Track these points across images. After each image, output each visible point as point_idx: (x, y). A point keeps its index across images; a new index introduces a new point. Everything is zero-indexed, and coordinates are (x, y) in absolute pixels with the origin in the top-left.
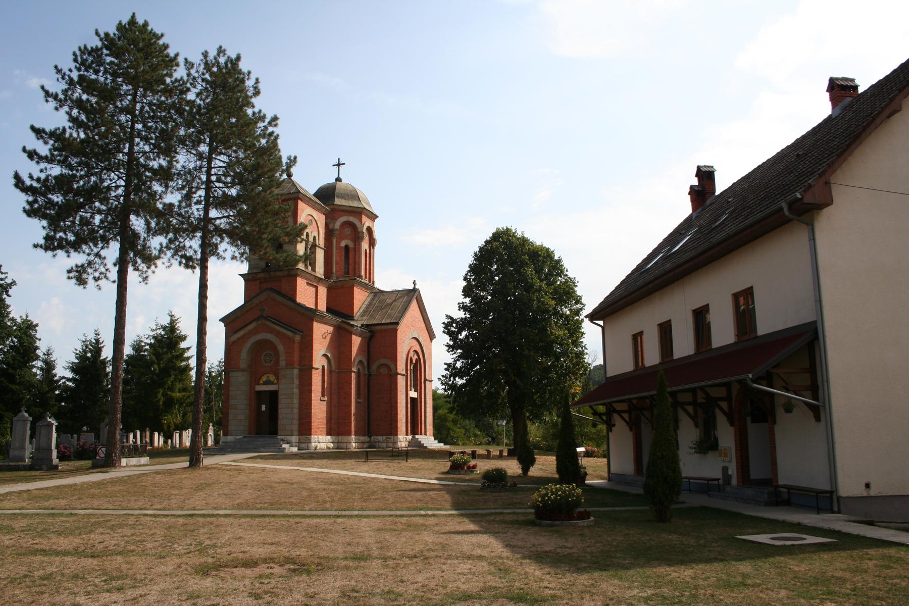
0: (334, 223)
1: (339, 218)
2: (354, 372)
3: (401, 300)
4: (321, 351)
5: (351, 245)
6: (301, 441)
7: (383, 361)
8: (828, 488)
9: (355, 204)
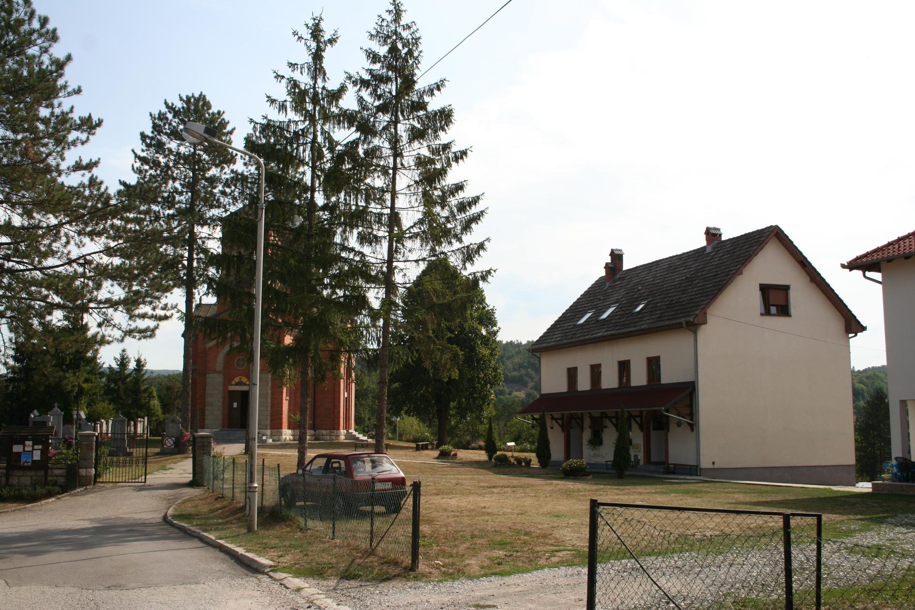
8: (695, 464)
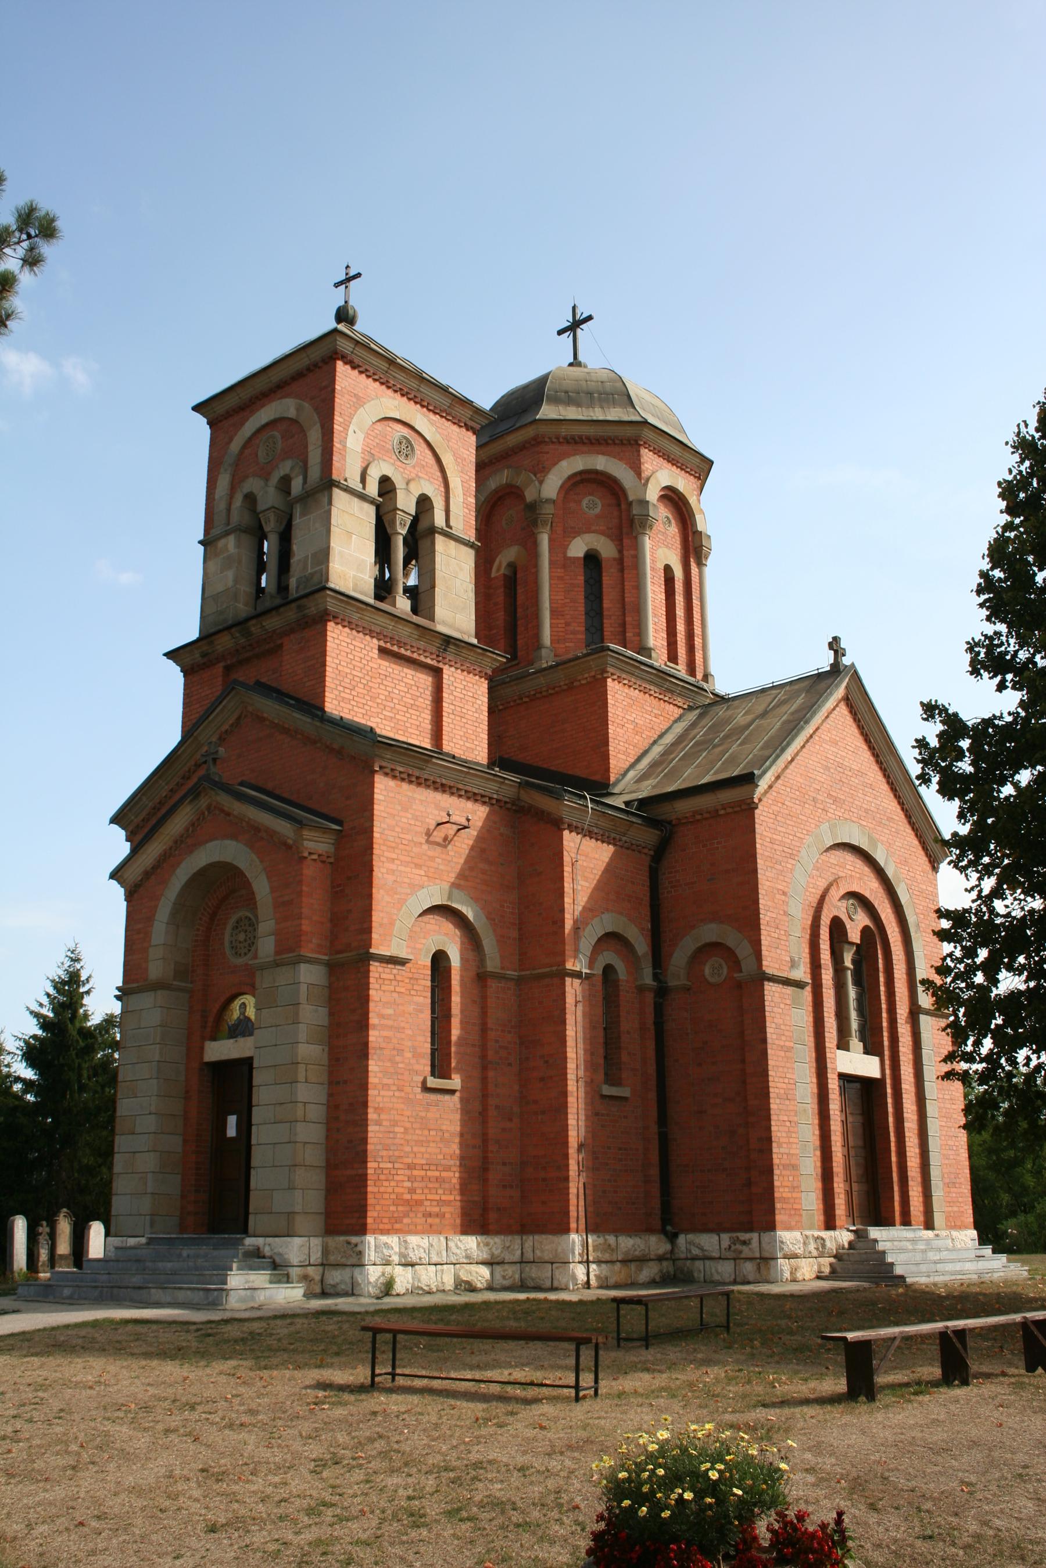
0: (541, 482)
1: (555, 464)
2: (577, 975)
3: (784, 709)
4: (422, 894)
5: (606, 549)
6: (332, 1259)
7: (710, 932)
9: (614, 414)
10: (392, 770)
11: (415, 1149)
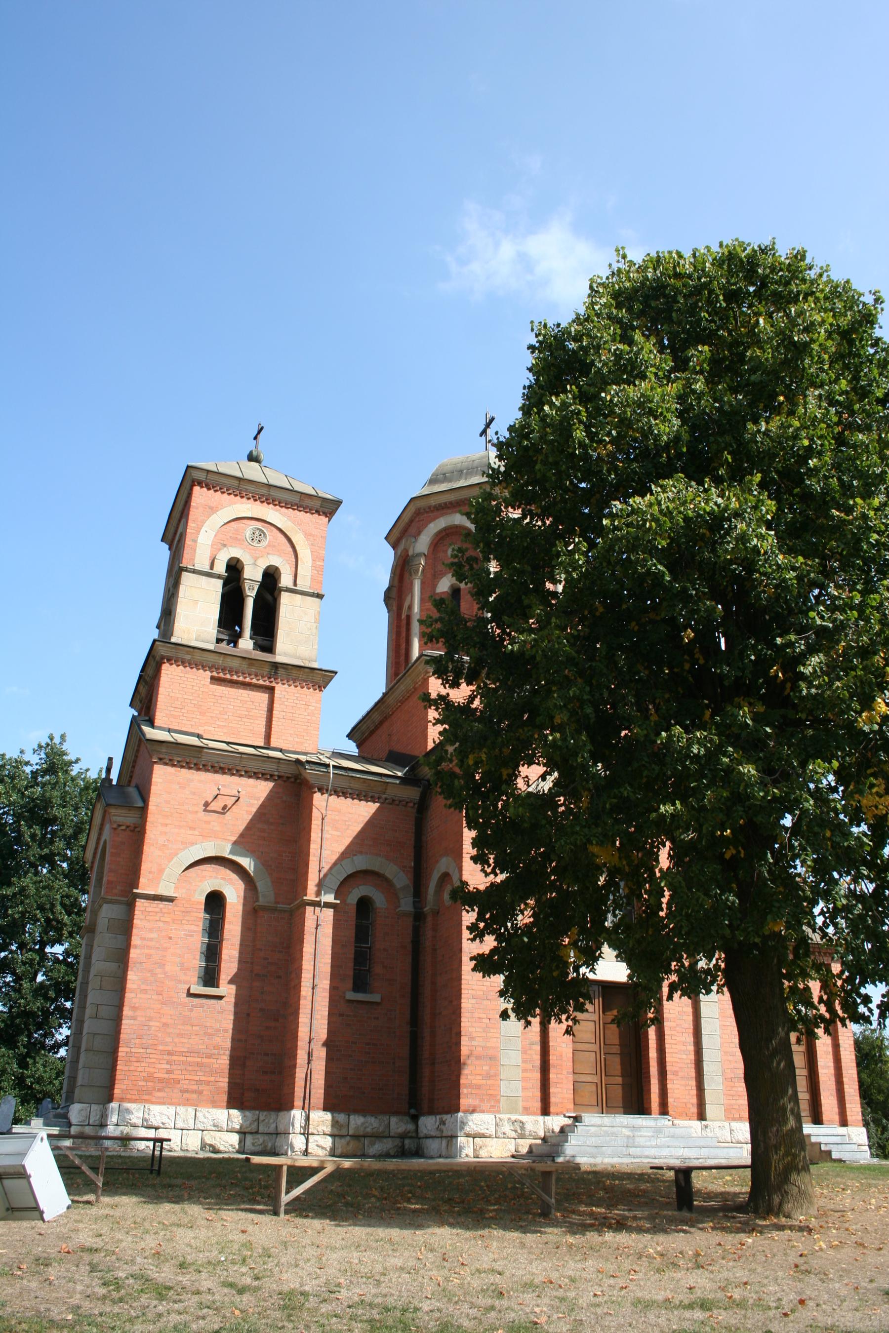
10: (170, 760)
11: (176, 1040)
